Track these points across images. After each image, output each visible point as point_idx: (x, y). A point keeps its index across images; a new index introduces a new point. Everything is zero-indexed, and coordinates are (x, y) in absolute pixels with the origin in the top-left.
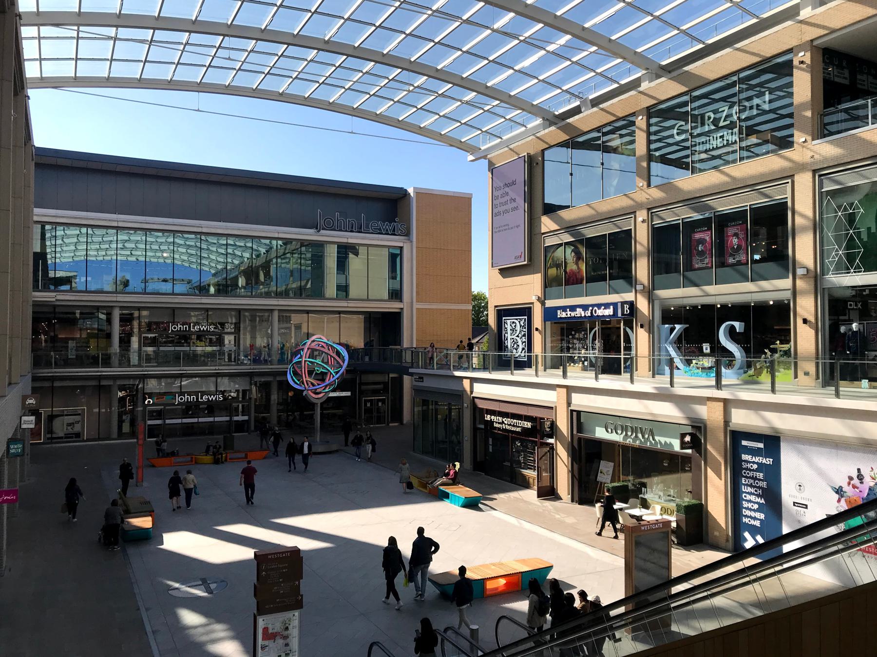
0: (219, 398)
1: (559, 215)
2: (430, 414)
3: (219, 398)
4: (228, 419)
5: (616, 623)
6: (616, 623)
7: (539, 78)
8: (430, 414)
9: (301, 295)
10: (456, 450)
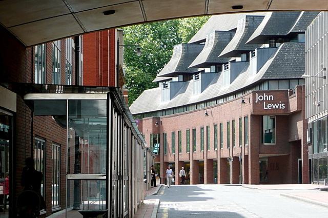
0: (282, 107)
3: (282, 107)
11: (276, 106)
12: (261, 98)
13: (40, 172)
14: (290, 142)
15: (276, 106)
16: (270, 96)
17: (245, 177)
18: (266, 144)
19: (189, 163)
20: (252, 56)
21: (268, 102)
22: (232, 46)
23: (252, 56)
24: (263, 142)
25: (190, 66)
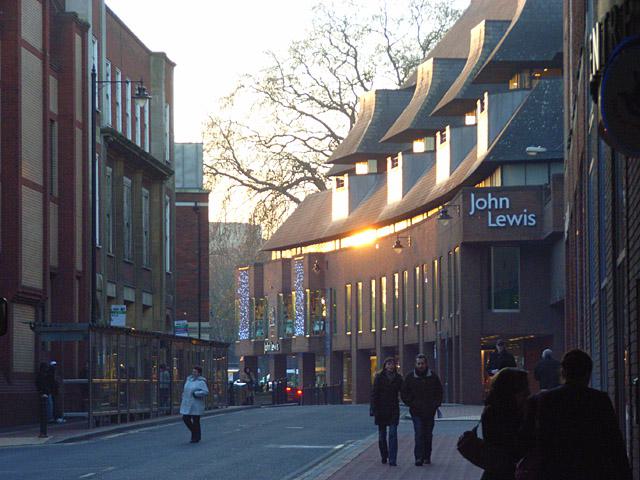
0: (528, 221)
1: (479, 404)
2: (566, 95)
3: (528, 221)
4: (198, 204)
5: (569, 21)
6: (569, 21)
7: (202, 335)
8: (566, 95)
9: (227, 345)
10: (231, 379)
11: (514, 219)
12: (481, 204)
13: (604, 396)
14: (552, 306)
15: (514, 219)
16: (501, 200)
17: (358, 367)
18: (496, 311)
19: (398, 347)
20: (393, 166)
21: (496, 212)
22: (405, 120)
23: (393, 166)
24: (490, 308)
25: (388, 135)
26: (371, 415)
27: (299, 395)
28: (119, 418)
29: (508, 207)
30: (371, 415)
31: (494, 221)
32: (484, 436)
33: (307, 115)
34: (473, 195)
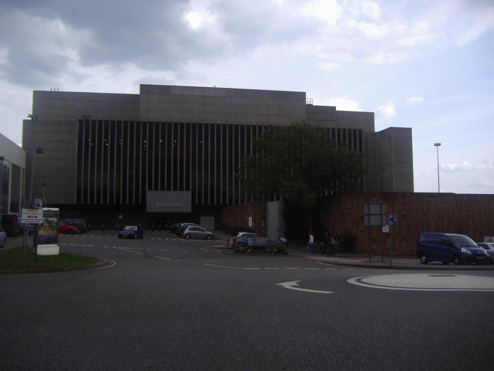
0: (180, 205)
3: (180, 205)
12: (160, 205)
26: (143, 87)
27: (159, 226)
28: (237, 174)
29: (167, 206)
30: (143, 87)
31: (170, 205)
32: (58, 208)
33: (7, 160)
34: (157, 203)
